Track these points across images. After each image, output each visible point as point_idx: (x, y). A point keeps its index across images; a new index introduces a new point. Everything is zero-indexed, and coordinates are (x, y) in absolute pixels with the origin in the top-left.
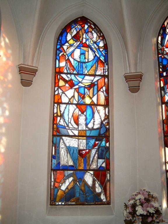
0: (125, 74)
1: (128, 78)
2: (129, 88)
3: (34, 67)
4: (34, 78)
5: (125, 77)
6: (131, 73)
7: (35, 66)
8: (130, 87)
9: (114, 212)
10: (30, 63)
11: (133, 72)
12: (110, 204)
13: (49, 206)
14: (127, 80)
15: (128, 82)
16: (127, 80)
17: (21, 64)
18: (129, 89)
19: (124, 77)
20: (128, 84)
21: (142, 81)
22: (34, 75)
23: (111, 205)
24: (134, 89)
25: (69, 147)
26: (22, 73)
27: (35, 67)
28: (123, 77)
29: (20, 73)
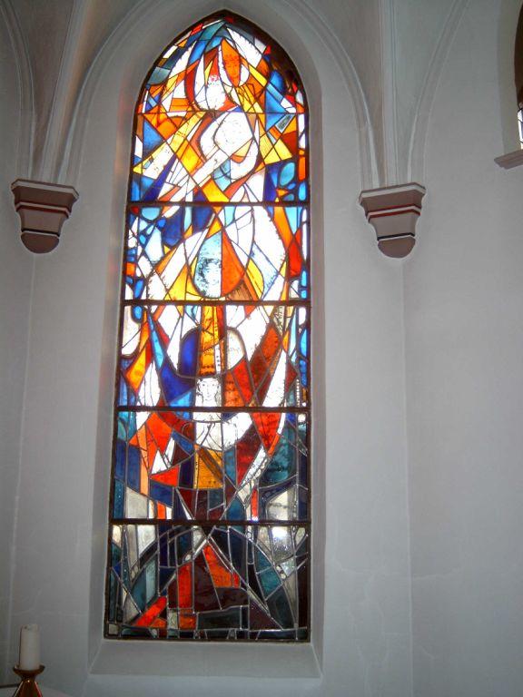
0: (363, 192)
1: (375, 207)
2: (23, 230)
3: (44, 183)
4: (66, 222)
5: (364, 203)
6: (384, 189)
7: (63, 184)
8: (383, 237)
9: (318, 666)
10: (398, 177)
11: (45, 180)
12: (309, 641)
13: (103, 640)
14: (370, 214)
15: (25, 211)
16: (370, 214)
17: (19, 180)
18: (22, 236)
19: (361, 204)
20: (23, 218)
21: (422, 212)
22: (65, 213)
23: (311, 644)
24: (397, 244)
25: (123, 443)
26: (412, 213)
27: (49, 184)
28: (10, 190)
29: (18, 210)
